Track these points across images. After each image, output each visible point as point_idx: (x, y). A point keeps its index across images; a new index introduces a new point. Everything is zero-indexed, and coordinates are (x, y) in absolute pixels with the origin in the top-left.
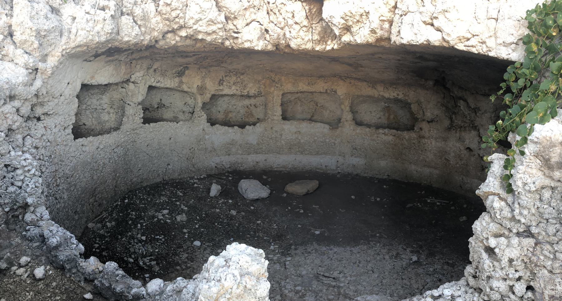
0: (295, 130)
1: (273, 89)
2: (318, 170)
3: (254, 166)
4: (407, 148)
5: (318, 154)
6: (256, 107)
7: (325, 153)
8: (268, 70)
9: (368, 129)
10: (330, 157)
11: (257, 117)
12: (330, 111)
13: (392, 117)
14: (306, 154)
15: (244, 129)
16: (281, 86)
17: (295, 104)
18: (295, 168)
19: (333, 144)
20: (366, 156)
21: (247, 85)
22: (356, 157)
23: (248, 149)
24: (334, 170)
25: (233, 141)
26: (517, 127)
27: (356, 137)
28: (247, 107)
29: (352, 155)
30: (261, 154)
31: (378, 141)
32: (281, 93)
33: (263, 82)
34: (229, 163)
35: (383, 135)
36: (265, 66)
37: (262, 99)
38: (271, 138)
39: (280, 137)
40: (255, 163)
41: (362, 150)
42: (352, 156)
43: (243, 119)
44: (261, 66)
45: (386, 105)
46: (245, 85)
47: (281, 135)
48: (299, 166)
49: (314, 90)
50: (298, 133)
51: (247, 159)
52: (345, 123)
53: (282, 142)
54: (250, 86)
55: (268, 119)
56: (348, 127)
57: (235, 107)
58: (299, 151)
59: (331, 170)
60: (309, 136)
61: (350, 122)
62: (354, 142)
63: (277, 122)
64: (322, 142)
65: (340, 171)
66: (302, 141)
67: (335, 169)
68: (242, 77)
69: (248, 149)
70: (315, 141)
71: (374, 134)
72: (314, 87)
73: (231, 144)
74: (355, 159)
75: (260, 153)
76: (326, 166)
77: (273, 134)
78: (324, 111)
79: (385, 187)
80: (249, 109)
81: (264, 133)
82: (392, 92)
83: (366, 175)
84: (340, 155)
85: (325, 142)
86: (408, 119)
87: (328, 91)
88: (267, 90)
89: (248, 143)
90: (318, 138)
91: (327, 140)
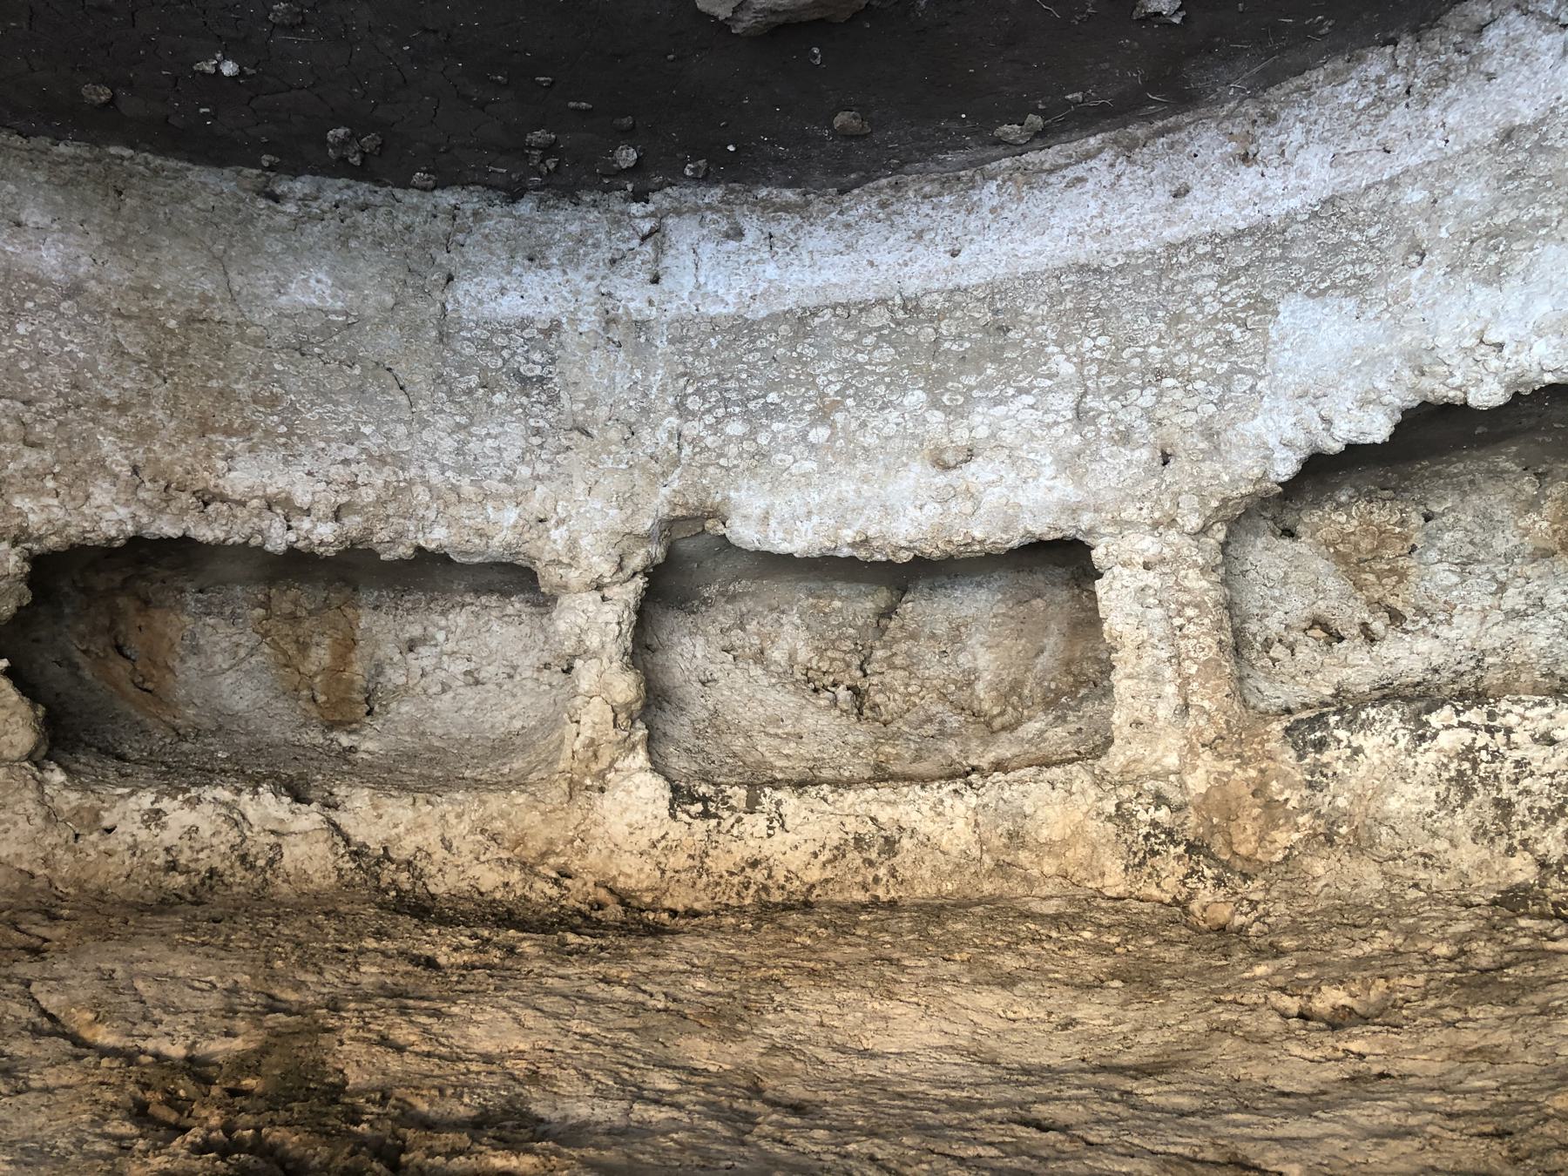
0: (978, 472)
1: (1197, 783)
2: (790, 195)
3: (1272, 119)
4: (104, 403)
5: (801, 322)
6: (1317, 622)
7: (742, 329)
8: (1259, 954)
9: (437, 537)
10: (714, 310)
11: (1302, 546)
12: (760, 657)
13: (321, 655)
14: (882, 302)
15: (1412, 401)
16: (1122, 816)
17: (1016, 687)
18: (946, 185)
19: (693, 403)
20: (443, 337)
21: (1443, 802)
22: (524, 324)
23: (1336, 249)
24: (678, 213)
25: (1499, 267)
26: (735, 755)
27: (524, 471)
28: (1396, 617)
29: (547, 333)
30: (1226, 228)
31: (352, 452)
32: (1116, 758)
33: (1283, 838)
34: (1491, 65)
35: (302, 498)
36: (1292, 1004)
37: (1275, 694)
38: (1160, 374)
39: (1090, 402)
40: (1265, 149)
41: (474, 380)
42: (554, 327)
43: (1416, 519)
44: (1331, 998)
45: (345, 740)
46: (1468, 792)
47: (1081, 415)
48: (926, 208)
49: (851, 796)
50: (949, 457)
51: (1335, 161)
52: (606, 568)
53: (1067, 369)
54: (1410, 790)
55: (1204, 530)
56: (585, 542)
57: (1513, 599)
58: (936, 317)
59: (696, 210)
60: (870, 440)
61: (573, 576)
62: (538, 432)
63: (1130, 513)
64: (772, 412)
65: (635, 208)
66: (916, 398)
67: (670, 221)
68: (1522, 870)
69: (1336, 249)
70: (823, 415)
71: (381, 502)
72: (852, 825)
73: (1511, 232)
74: (528, 311)
75: (1238, 235)
76: (738, 234)
77: (1147, 413)
78: (804, 654)
79: (229, 68)
80: (1376, 605)
81: (1219, 404)
82: (206, 830)
83: (447, 198)
84: (641, 325)
85: (748, 416)
86: (196, 650)
87: (739, 795)
88: (1245, 763)
89: (1351, 292)
90: (804, 436)
91: (735, 428)
